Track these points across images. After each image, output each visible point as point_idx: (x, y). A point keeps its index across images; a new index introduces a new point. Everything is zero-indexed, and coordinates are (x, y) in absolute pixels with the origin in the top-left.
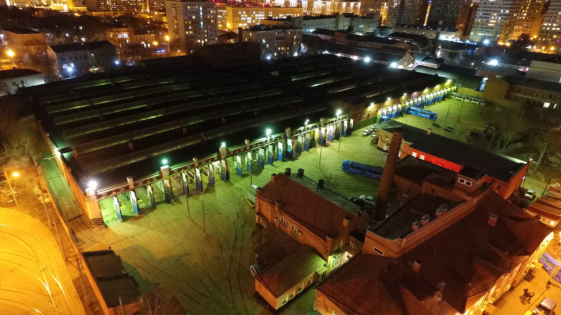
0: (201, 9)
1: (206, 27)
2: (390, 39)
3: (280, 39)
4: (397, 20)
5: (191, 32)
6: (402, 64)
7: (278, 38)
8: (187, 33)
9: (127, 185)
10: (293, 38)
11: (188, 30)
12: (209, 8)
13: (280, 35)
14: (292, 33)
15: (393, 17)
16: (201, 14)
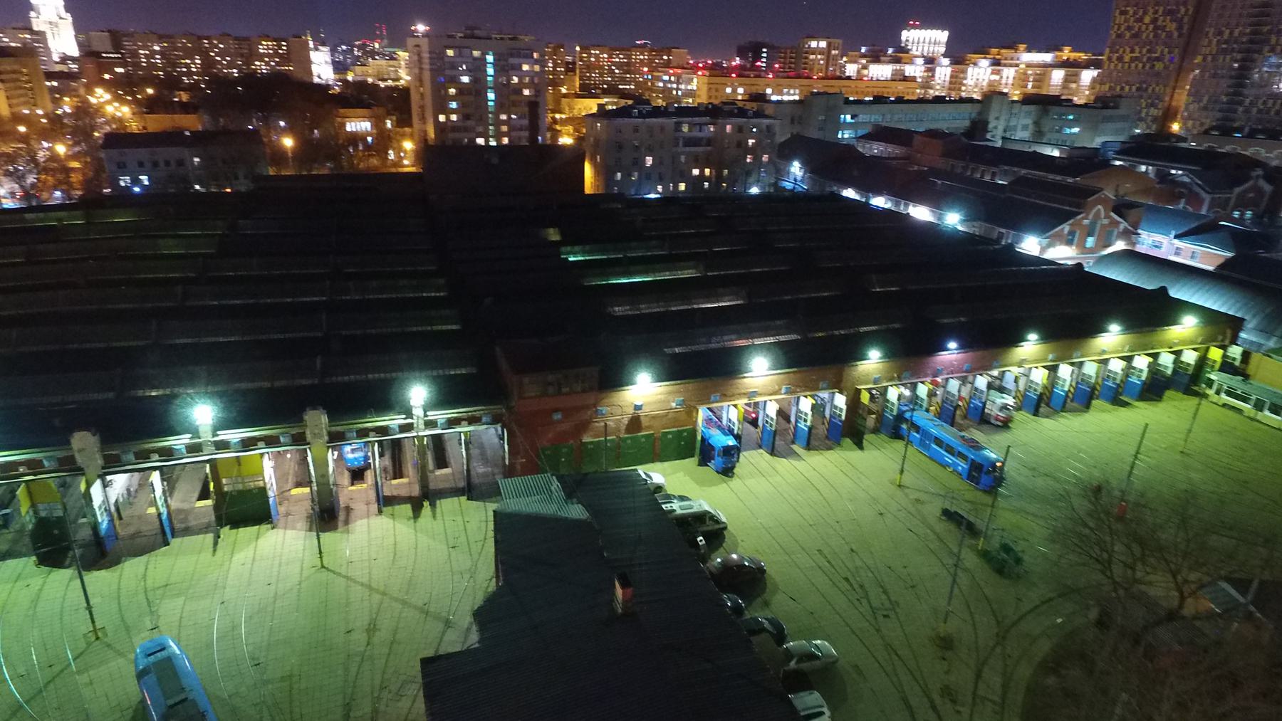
0: (490, 58)
1: (501, 106)
2: (1118, 163)
3: (695, 145)
4: (1219, 115)
5: (454, 117)
6: (1069, 243)
7: (691, 142)
8: (442, 118)
9: (409, 421)
10: (741, 145)
11: (448, 112)
12: (519, 56)
13: (696, 134)
14: (740, 129)
15: (1205, 108)
16: (490, 71)
